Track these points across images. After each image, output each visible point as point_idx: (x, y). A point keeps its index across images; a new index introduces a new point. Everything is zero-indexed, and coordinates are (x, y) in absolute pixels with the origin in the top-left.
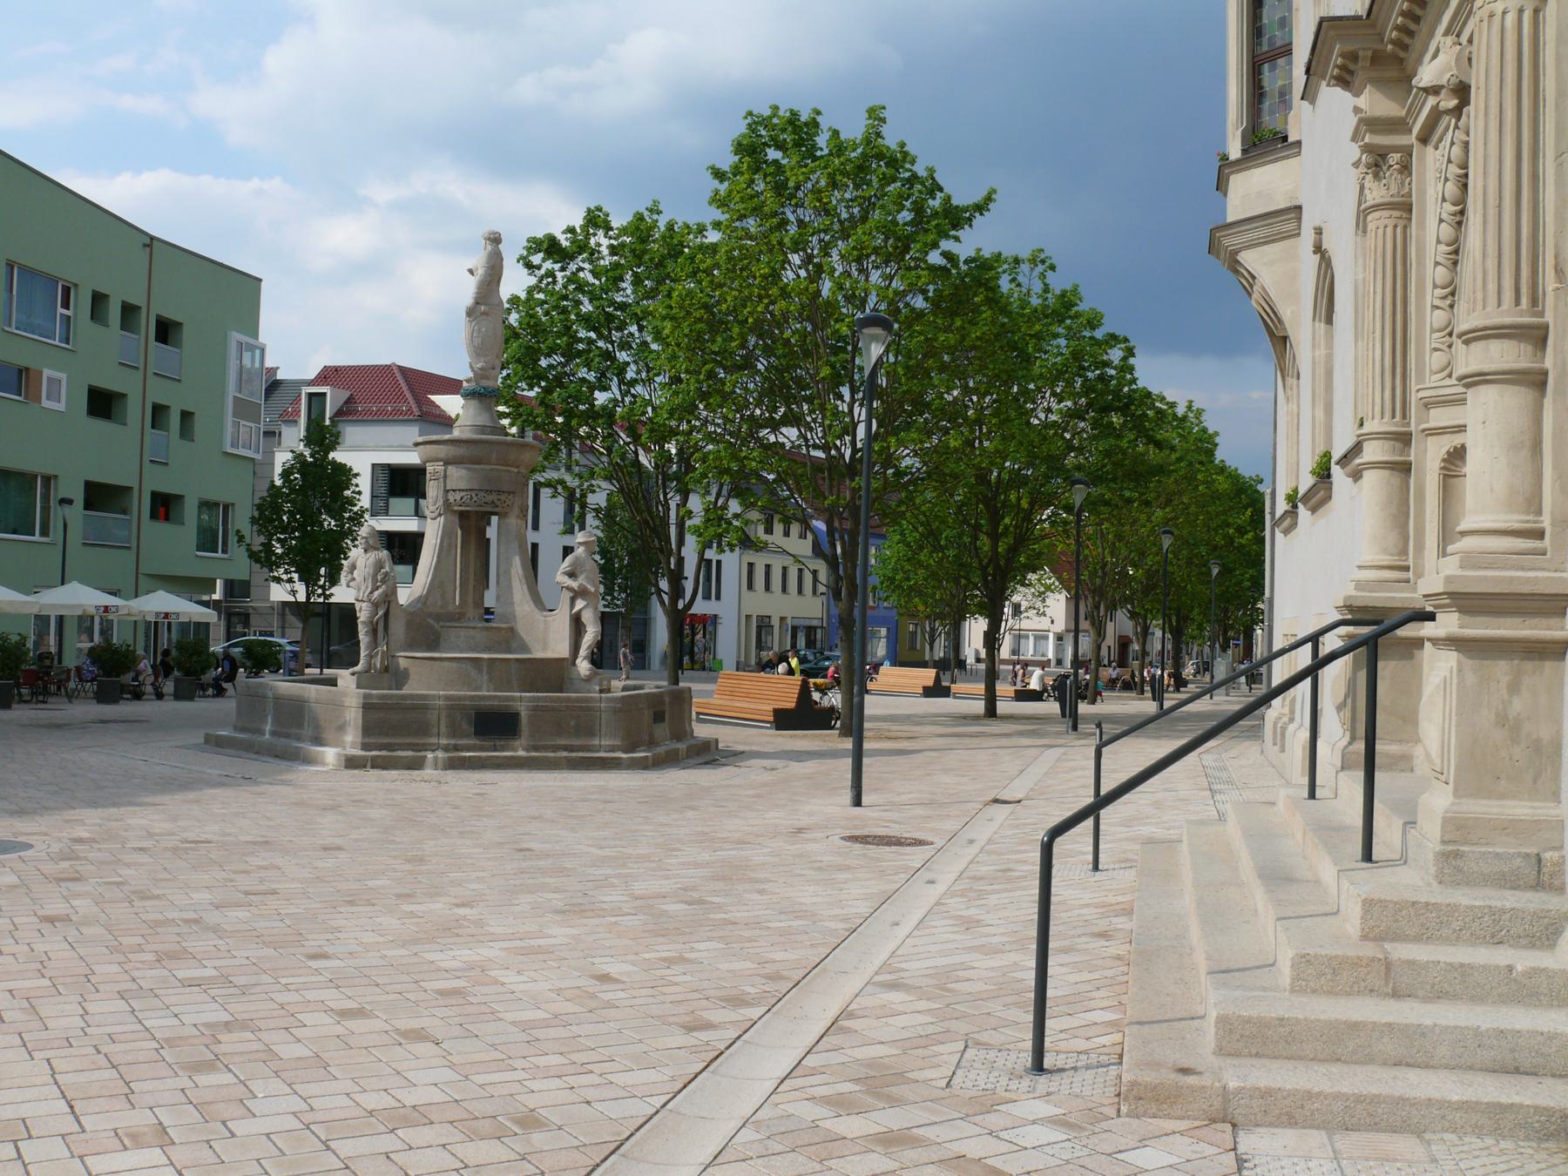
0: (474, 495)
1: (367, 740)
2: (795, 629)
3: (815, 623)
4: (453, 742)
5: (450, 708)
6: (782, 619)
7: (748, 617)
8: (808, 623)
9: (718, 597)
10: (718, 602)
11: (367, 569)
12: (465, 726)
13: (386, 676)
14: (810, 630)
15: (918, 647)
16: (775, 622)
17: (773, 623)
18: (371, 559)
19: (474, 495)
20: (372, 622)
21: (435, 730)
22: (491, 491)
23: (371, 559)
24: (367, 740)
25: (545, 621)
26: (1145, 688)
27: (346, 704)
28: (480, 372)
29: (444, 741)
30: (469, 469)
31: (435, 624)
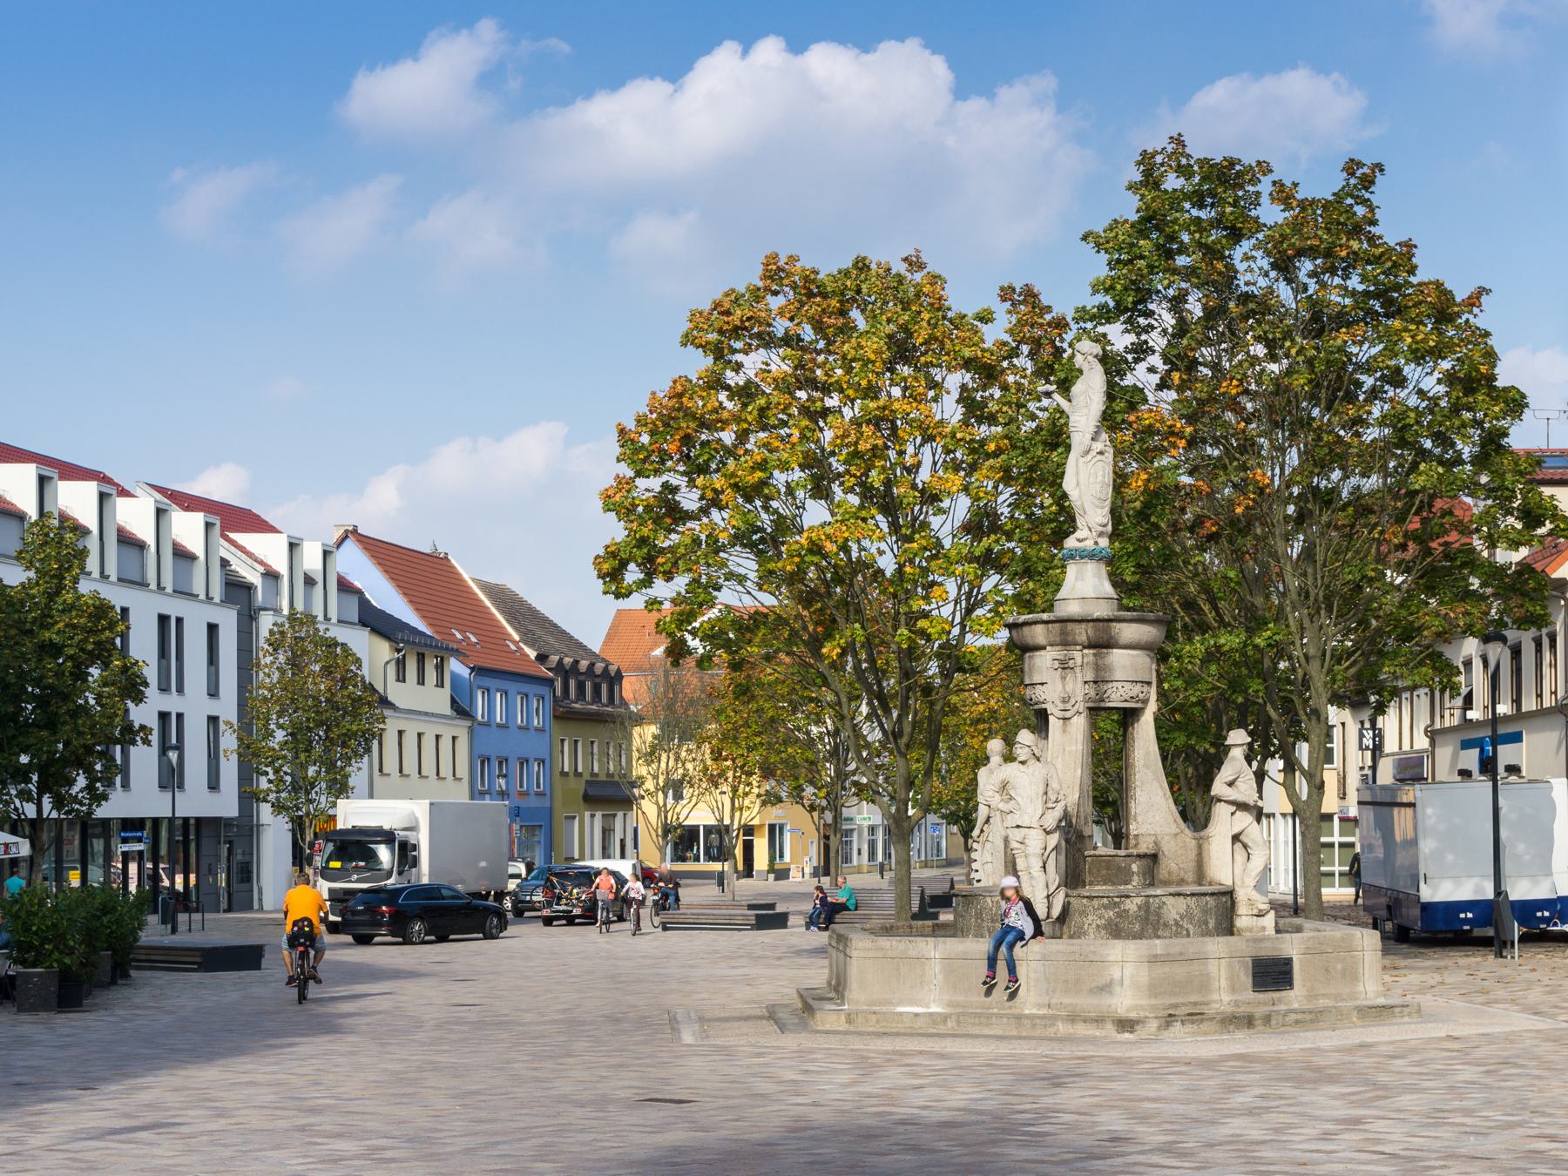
1: (1196, 967)
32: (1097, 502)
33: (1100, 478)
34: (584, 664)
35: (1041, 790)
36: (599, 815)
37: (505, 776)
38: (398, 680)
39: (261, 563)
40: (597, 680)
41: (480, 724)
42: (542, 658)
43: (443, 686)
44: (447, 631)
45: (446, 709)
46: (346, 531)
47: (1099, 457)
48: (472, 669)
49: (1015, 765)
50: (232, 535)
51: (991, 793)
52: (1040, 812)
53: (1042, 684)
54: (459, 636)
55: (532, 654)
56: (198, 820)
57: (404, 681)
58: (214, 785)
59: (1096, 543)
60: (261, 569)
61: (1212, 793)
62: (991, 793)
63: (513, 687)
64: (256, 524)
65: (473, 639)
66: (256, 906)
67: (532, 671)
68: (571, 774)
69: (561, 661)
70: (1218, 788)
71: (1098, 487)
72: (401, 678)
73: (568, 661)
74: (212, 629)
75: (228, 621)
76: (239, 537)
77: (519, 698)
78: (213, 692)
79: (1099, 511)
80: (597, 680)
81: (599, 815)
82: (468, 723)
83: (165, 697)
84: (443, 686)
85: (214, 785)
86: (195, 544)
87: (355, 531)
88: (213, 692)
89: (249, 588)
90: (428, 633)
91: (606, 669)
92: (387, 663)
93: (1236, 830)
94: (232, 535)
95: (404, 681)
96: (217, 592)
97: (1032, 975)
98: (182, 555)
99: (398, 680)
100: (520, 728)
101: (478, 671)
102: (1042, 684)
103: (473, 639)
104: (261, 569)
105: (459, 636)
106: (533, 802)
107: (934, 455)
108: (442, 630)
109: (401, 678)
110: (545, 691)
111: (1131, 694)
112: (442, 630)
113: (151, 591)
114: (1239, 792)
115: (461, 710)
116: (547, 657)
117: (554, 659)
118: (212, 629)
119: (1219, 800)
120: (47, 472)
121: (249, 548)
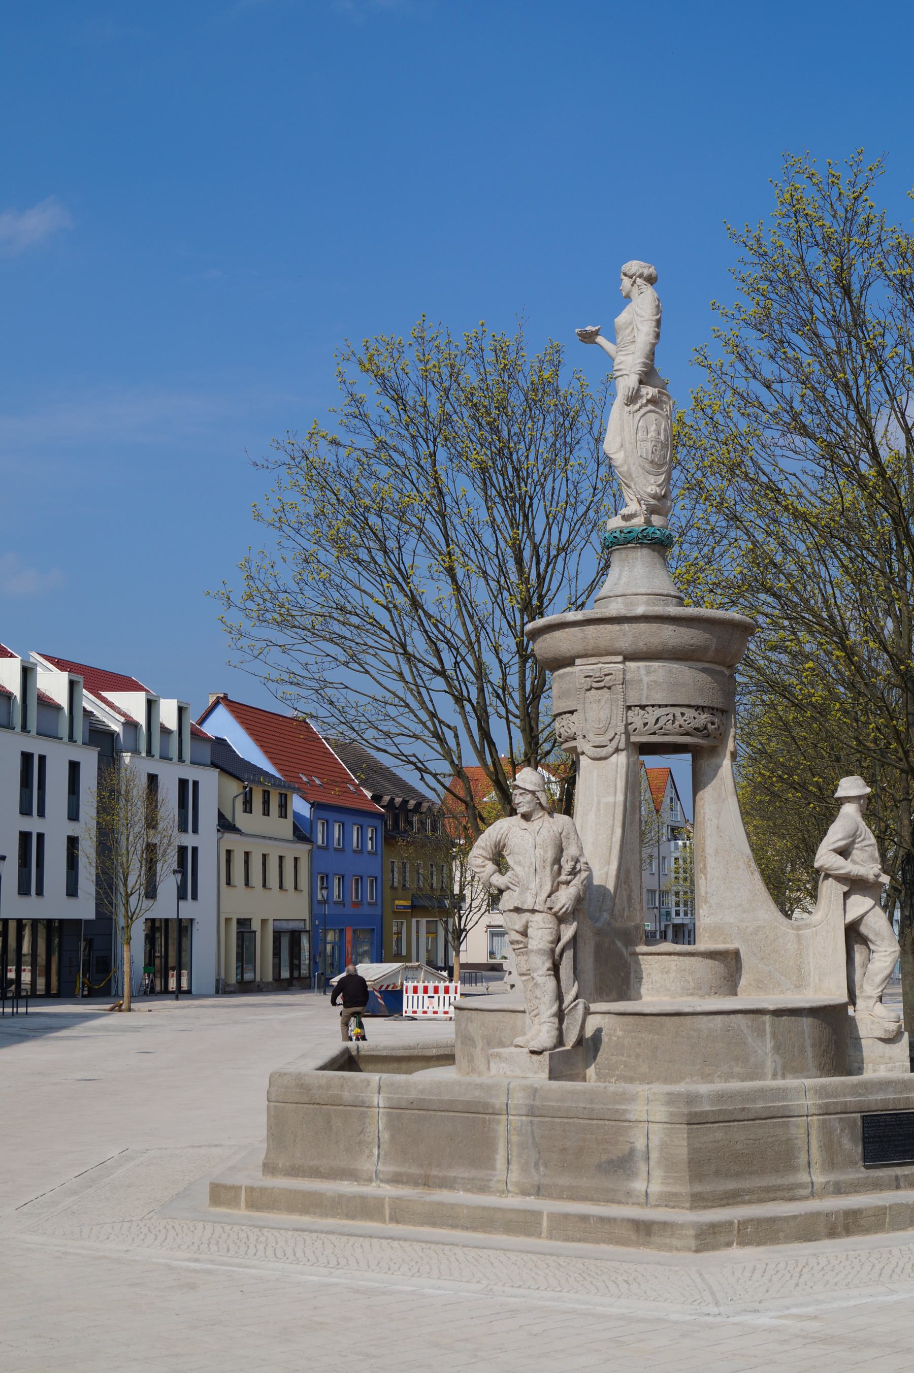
0: (678, 715)
1: (698, 1188)
2: (277, 935)
3: (299, 926)
4: (832, 1177)
5: (826, 1111)
6: (264, 922)
7: (228, 920)
8: (291, 926)
9: (40, 892)
10: (195, 902)
11: (539, 851)
12: (847, 1144)
13: (580, 1049)
14: (295, 936)
15: (404, 953)
16: (256, 926)
17: (254, 928)
18: (544, 832)
19: (678, 715)
20: (553, 951)
21: (803, 1159)
22: (703, 708)
23: (544, 832)
24: (698, 1188)
25: (799, 937)
26: (29, 987)
27: (631, 1117)
28: (653, 502)
29: (819, 1178)
30: (704, 670)
31: (624, 949)
32: (648, 466)
33: (652, 434)
34: (412, 803)
35: (550, 855)
36: (423, 921)
37: (327, 888)
38: (245, 811)
39: (124, 715)
40: (397, 811)
41: (319, 847)
42: (377, 798)
43: (286, 817)
44: (296, 775)
45: (289, 833)
46: (218, 698)
47: (650, 407)
48: (313, 805)
49: (516, 819)
50: (104, 694)
51: (479, 861)
52: (547, 888)
53: (572, 712)
54: (305, 779)
55: (369, 795)
56: (61, 921)
57: (268, 815)
58: (72, 890)
59: (648, 522)
60: (122, 719)
61: (817, 865)
62: (479, 861)
63: (349, 819)
64: (127, 684)
65: (318, 782)
66: (113, 993)
67: (366, 807)
68: (400, 889)
69: (392, 800)
70: (825, 857)
71: (650, 446)
72: (248, 807)
73: (398, 800)
74: (74, 767)
75: (89, 760)
76: (107, 695)
77: (355, 828)
78: (74, 815)
79: (652, 479)
80: (397, 811)
81: (423, 921)
82: (309, 847)
83: (26, 819)
84: (286, 817)
85: (72, 890)
86: (61, 697)
87: (225, 698)
88: (74, 815)
89: (112, 735)
90: (277, 775)
91: (430, 809)
92: (236, 797)
93: (851, 916)
94: (104, 694)
95: (268, 815)
96: (79, 734)
97: (514, 1138)
98: (45, 703)
99: (245, 811)
100: (354, 851)
101: (316, 806)
102: (572, 712)
103: (318, 782)
104: (122, 719)
105: (305, 779)
106: (366, 910)
107: (548, 517)
108: (288, 773)
109: (248, 807)
110: (378, 823)
111: (695, 724)
112: (288, 773)
113: (143, 758)
114: (854, 862)
115: (301, 834)
116: (381, 797)
117: (387, 798)
118: (74, 767)
119: (827, 876)
120: (76, 677)
121: (116, 704)
